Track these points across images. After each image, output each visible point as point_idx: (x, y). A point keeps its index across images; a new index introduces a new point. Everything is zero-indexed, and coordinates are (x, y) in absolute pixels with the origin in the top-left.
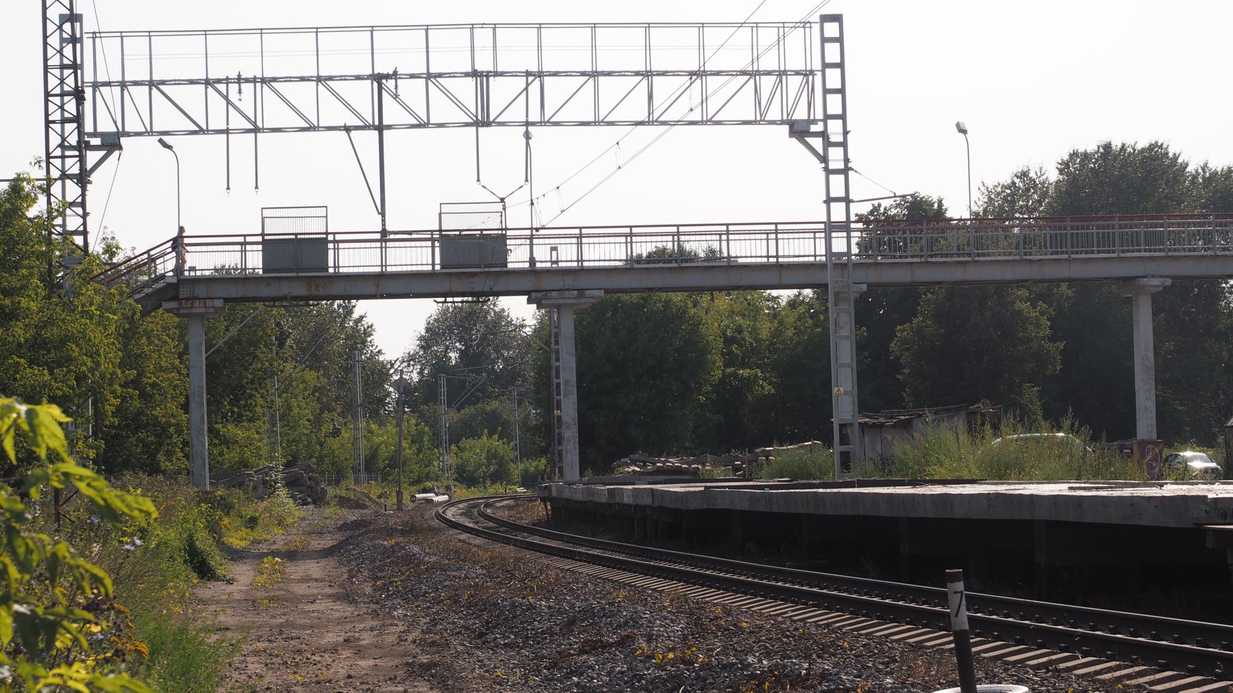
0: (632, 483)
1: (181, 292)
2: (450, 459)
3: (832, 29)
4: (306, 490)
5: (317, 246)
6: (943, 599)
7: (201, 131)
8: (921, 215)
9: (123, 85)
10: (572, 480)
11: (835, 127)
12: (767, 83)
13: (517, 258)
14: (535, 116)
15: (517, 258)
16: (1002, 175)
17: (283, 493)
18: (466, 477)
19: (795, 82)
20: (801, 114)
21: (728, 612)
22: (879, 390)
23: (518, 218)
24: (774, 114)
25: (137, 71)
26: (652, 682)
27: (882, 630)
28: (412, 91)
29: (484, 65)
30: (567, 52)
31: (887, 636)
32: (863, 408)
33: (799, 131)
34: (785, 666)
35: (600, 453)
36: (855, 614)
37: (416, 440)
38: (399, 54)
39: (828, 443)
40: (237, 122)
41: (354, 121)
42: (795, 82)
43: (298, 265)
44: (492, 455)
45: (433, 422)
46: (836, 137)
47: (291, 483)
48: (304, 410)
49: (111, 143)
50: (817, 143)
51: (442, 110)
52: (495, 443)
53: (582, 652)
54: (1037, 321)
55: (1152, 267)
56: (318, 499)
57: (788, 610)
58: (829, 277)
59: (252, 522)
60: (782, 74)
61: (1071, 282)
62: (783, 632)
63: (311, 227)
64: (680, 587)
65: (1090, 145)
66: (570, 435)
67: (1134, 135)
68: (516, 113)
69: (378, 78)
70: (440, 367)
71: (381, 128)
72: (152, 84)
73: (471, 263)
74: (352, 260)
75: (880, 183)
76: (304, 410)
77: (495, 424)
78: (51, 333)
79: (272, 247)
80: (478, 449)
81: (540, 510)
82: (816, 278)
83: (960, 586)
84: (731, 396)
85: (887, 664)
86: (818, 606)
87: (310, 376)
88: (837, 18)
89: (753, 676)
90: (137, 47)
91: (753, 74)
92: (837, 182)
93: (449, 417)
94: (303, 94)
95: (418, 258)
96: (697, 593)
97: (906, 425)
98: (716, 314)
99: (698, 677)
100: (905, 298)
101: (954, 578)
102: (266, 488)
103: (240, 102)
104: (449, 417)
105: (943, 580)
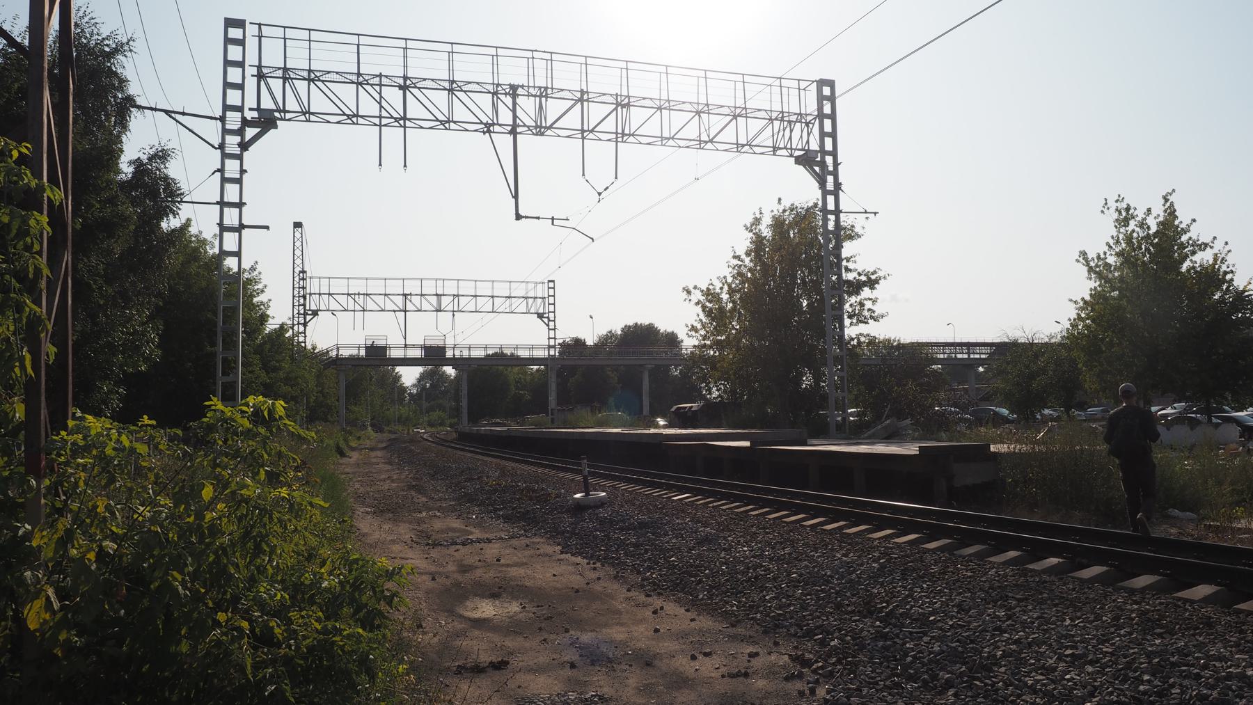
0: (485, 427)
2: (426, 419)
3: (551, 285)
4: (378, 428)
8: (578, 343)
10: (465, 426)
11: (551, 315)
12: (531, 301)
13: (449, 354)
15: (449, 354)
16: (603, 332)
18: (431, 424)
20: (541, 311)
22: (564, 399)
23: (450, 342)
28: (416, 299)
30: (467, 289)
33: (540, 316)
35: (474, 418)
43: (376, 354)
47: (373, 426)
51: (426, 306)
57: (532, 468)
59: (359, 438)
65: (631, 323)
66: (465, 411)
67: (644, 320)
69: (405, 295)
70: (423, 388)
75: (565, 333)
79: (367, 348)
80: (435, 415)
81: (455, 435)
92: (552, 333)
93: (425, 405)
95: (417, 353)
96: (503, 462)
102: (364, 427)
103: (359, 301)
104: (425, 405)
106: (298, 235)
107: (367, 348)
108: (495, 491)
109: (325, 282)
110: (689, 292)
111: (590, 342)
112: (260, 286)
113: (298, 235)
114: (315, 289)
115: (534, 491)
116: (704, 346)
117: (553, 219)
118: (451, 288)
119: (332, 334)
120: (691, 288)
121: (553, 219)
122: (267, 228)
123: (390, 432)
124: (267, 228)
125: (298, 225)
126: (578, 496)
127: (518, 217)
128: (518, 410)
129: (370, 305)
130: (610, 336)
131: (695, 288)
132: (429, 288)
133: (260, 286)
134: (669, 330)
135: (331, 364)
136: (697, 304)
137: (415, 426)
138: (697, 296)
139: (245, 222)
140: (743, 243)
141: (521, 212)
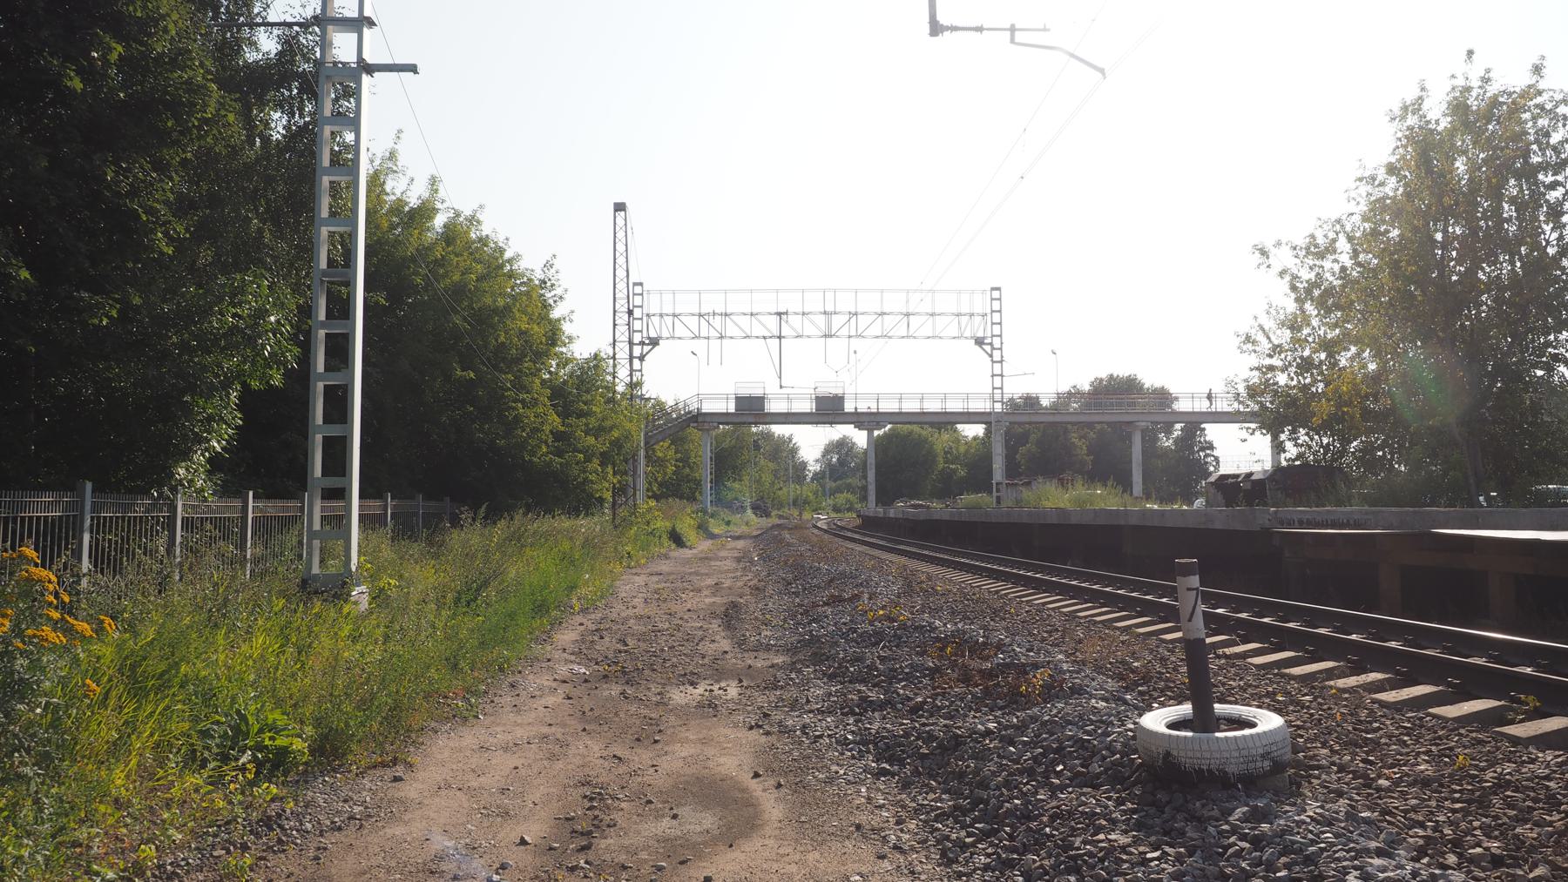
0: (901, 508)
1: (697, 419)
2: (830, 502)
3: (996, 294)
4: (760, 509)
5: (759, 401)
6: (1172, 592)
7: (696, 337)
8: (1031, 402)
9: (661, 315)
10: (872, 508)
11: (997, 342)
12: (964, 319)
13: (849, 407)
14: (853, 333)
15: (849, 407)
16: (1065, 387)
17: (749, 511)
18: (836, 509)
19: (978, 319)
20: (980, 334)
21: (929, 578)
22: (1012, 470)
23: (849, 390)
24: (968, 334)
25: (668, 309)
26: (861, 636)
27: (1040, 599)
28: (795, 321)
29: (829, 308)
30: (869, 303)
31: (1044, 604)
32: (1008, 476)
33: (980, 342)
34: (964, 633)
35: (885, 498)
36: (1016, 584)
37: (816, 493)
38: (790, 303)
39: (991, 492)
40: (713, 333)
41: (767, 334)
42: (978, 319)
43: (751, 408)
44: (848, 501)
45: (823, 486)
46: (997, 345)
47: (755, 508)
48: (767, 478)
49: (654, 342)
50: (988, 348)
51: (809, 329)
52: (849, 496)
53: (826, 604)
54: (1081, 446)
55: (1141, 417)
56: (768, 515)
57: (967, 577)
58: (992, 419)
59: (728, 523)
60: (972, 315)
61: (1108, 424)
62: (965, 595)
63: (757, 392)
64: (903, 560)
65: (1104, 375)
66: (872, 489)
67: (1122, 371)
68: (844, 331)
69: (780, 314)
70: (829, 464)
71: (780, 337)
72: (674, 315)
73: (829, 410)
74: (773, 406)
75: (1016, 388)
76: (767, 478)
77: (849, 488)
78: (608, 423)
79: (739, 400)
80: (841, 498)
81: (859, 522)
82: (986, 419)
83: (1195, 581)
84: (947, 476)
85: (1049, 632)
86: (989, 577)
87: (770, 464)
88: (998, 289)
89: (938, 639)
90: (668, 297)
91: (958, 315)
92: (997, 367)
93: (830, 484)
94: (744, 321)
95: (807, 406)
96: (913, 564)
97: (1028, 484)
98: (941, 441)
99: (895, 635)
100: (1023, 439)
101: (1187, 571)
102: (742, 509)
103: (714, 323)
104: (830, 484)
105: (1172, 572)
106: (620, 222)
107: (739, 400)
108: (878, 637)
109: (668, 297)
110: (1264, 253)
111: (1045, 402)
112: (558, 291)
113: (620, 222)
114: (654, 308)
115: (977, 650)
116: (1271, 368)
117: (1013, 29)
118: (845, 304)
119: (682, 378)
120: (1269, 245)
121: (1013, 29)
122: (413, 69)
123: (780, 517)
124: (413, 69)
125: (620, 207)
126: (1156, 720)
127: (936, 28)
128: (948, 488)
129: (731, 330)
130: (1073, 395)
131: (1278, 244)
132: (814, 304)
133: (558, 291)
134: (1158, 385)
135: (688, 424)
136: (1282, 274)
137: (815, 510)
138: (1284, 258)
139: (369, 57)
140: (1380, 146)
141: (943, 19)
